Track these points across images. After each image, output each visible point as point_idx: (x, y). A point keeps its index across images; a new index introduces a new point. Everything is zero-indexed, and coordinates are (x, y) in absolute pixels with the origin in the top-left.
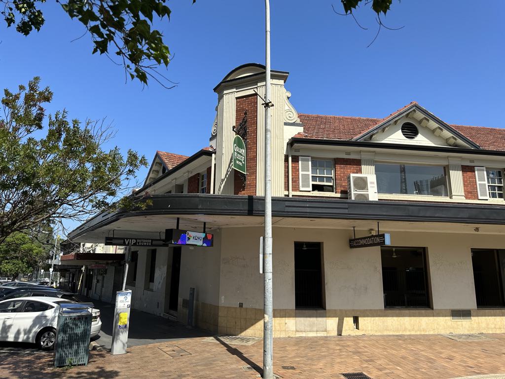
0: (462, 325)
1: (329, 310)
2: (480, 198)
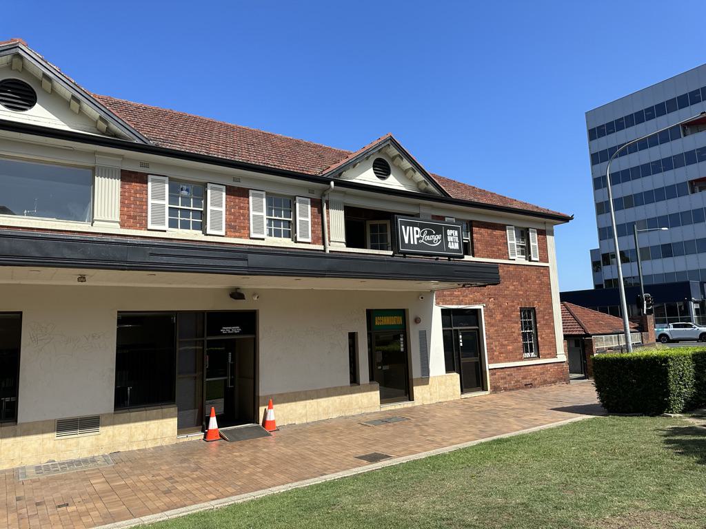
0: (78, 444)
2: (533, 259)
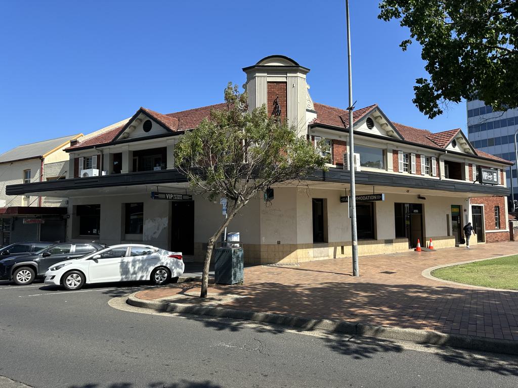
1: (330, 243)
2: (433, 175)
